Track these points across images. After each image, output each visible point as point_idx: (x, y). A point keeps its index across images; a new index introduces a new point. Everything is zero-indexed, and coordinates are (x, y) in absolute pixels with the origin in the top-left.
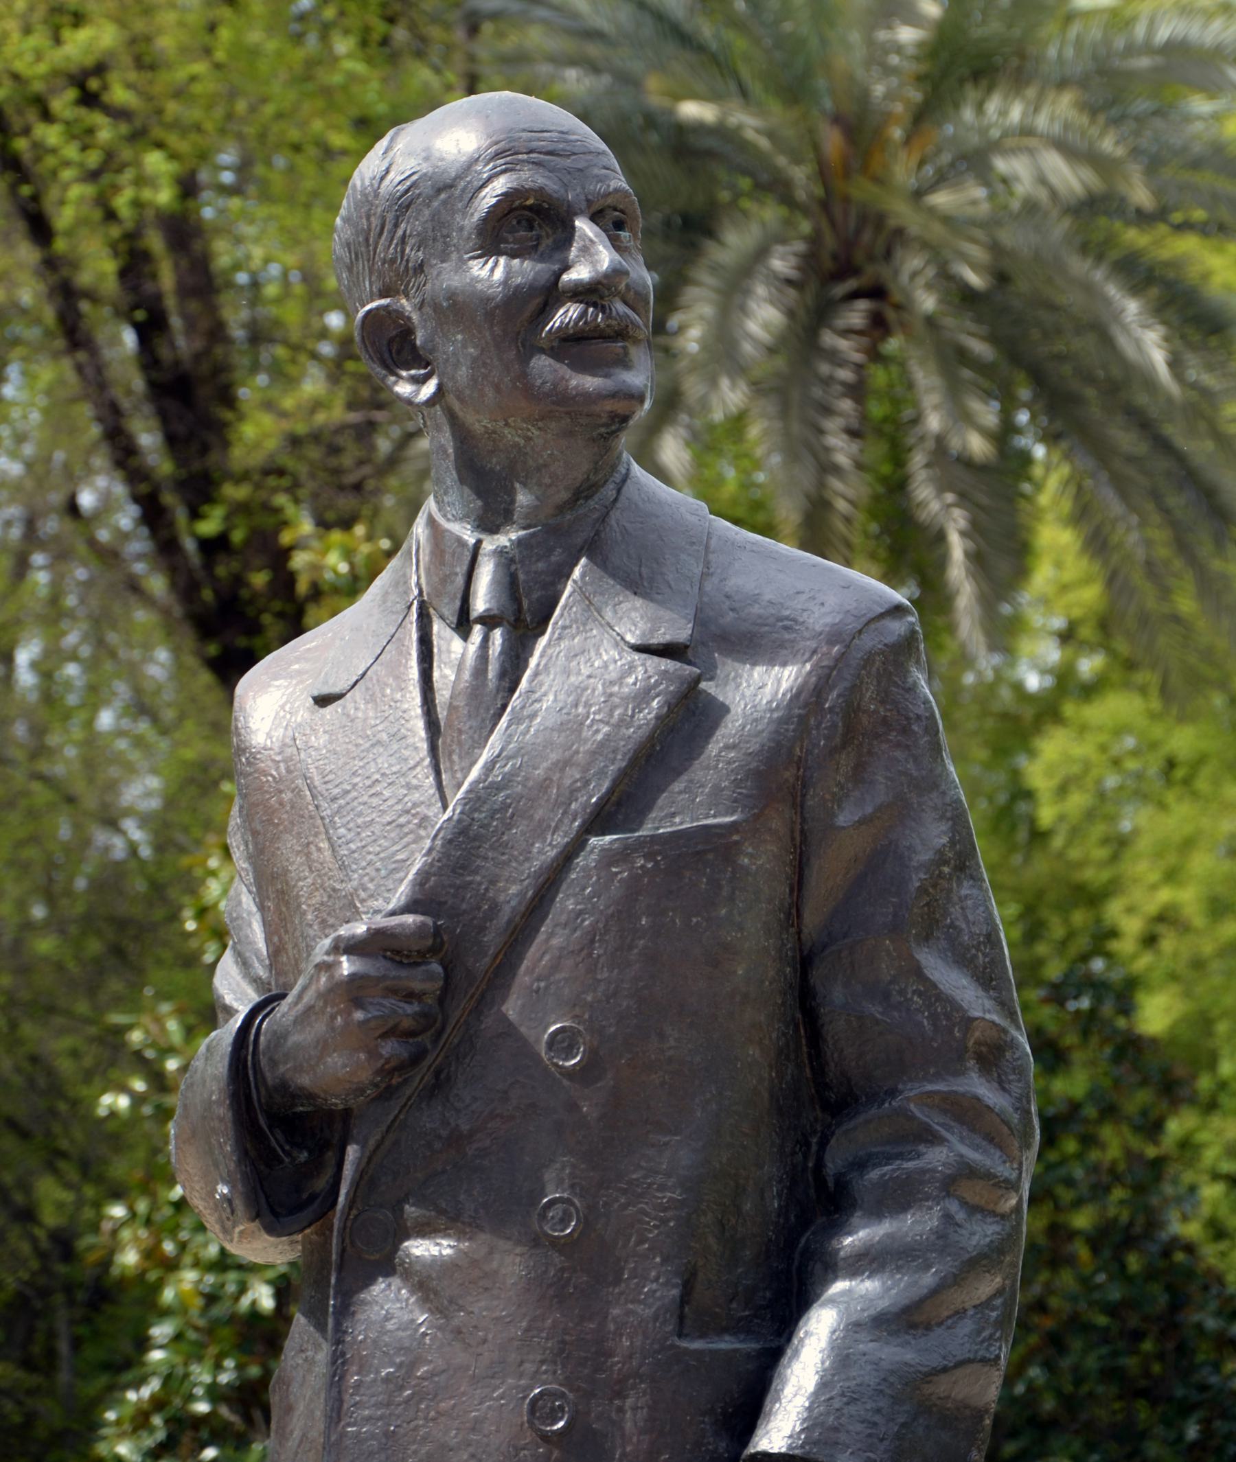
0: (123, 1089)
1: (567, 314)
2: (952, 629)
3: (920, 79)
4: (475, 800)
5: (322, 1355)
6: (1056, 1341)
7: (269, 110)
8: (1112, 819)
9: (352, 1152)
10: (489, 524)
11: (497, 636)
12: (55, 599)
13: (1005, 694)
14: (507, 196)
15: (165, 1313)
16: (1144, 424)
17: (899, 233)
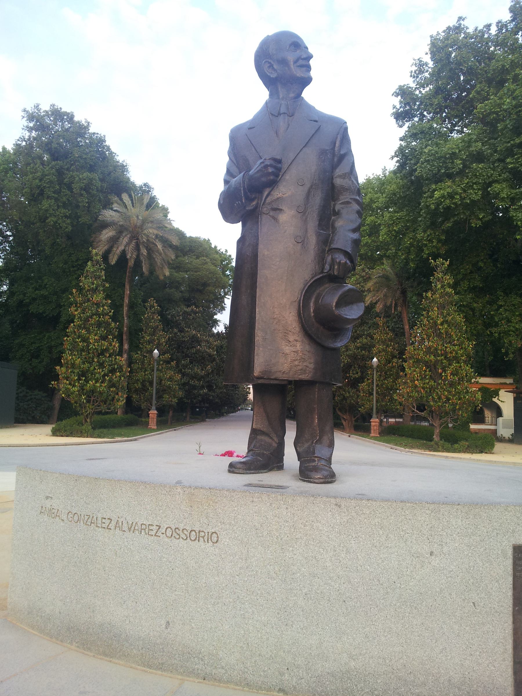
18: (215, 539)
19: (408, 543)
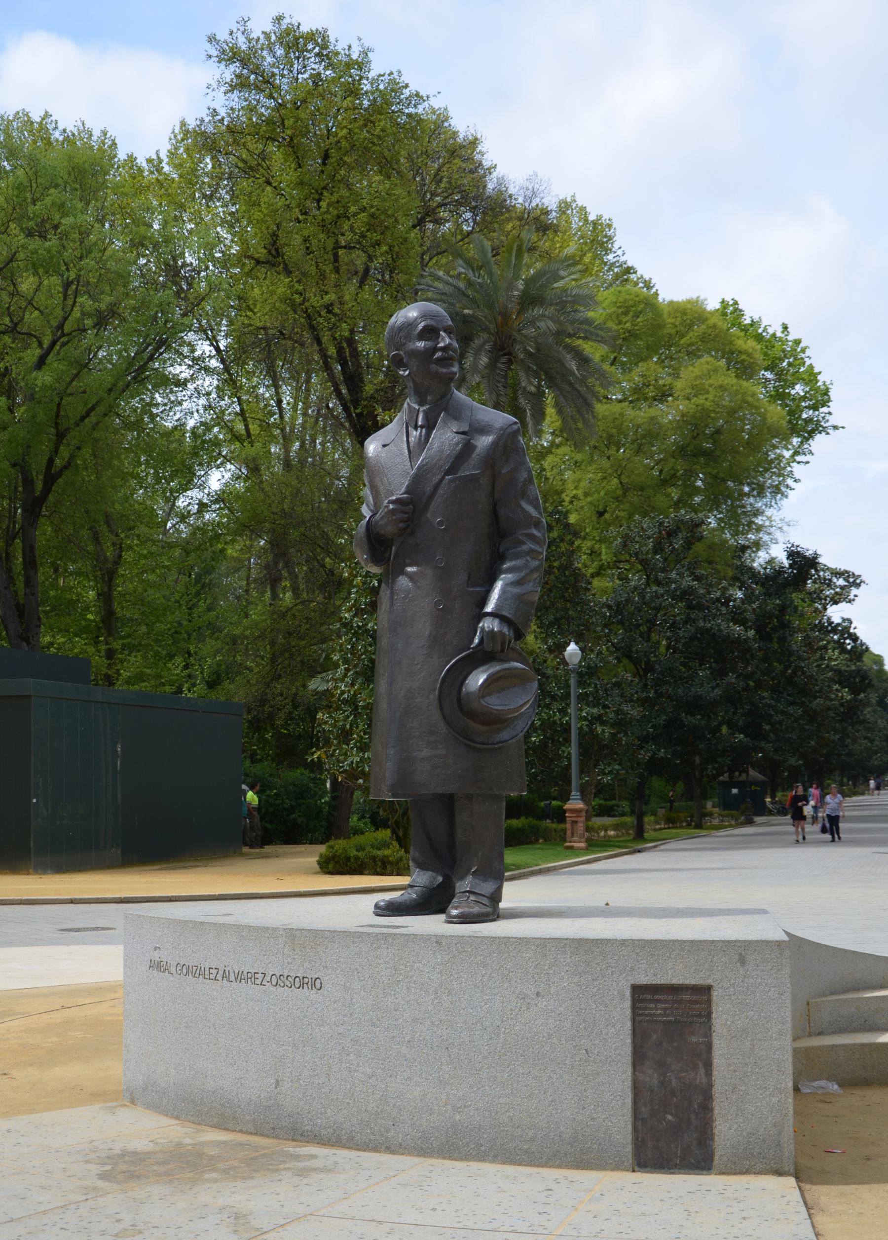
0: (343, 538)
1: (438, 354)
2: (527, 431)
3: (519, 304)
4: (419, 468)
5: (388, 592)
6: (550, 590)
7: (370, 313)
8: (563, 475)
9: (394, 548)
10: (421, 404)
11: (424, 430)
12: (324, 428)
13: (539, 447)
14: (424, 327)
15: (354, 587)
16: (570, 384)
17: (515, 339)
18: (318, 985)
19: (513, 983)
